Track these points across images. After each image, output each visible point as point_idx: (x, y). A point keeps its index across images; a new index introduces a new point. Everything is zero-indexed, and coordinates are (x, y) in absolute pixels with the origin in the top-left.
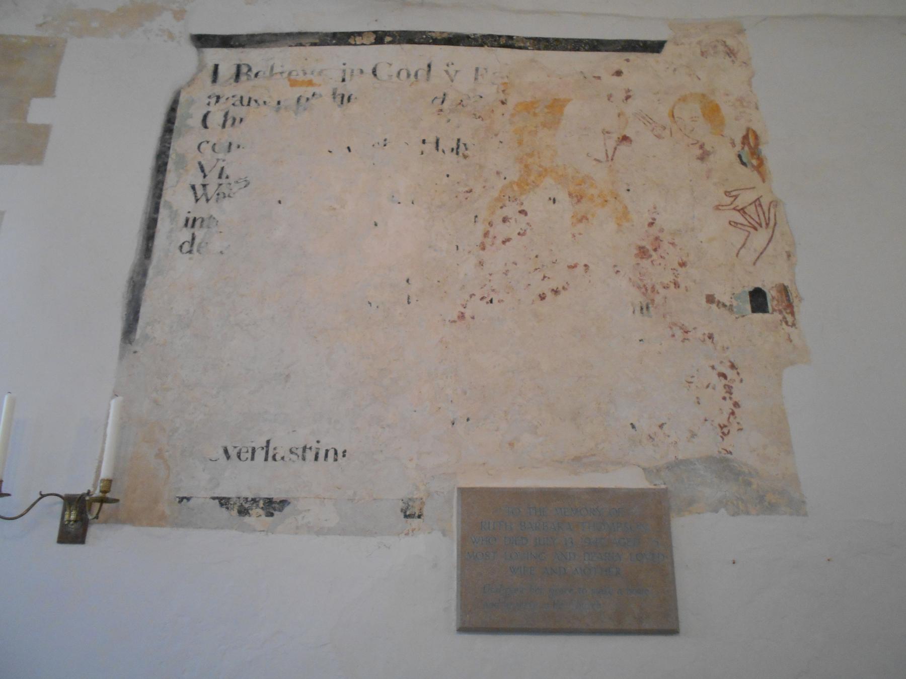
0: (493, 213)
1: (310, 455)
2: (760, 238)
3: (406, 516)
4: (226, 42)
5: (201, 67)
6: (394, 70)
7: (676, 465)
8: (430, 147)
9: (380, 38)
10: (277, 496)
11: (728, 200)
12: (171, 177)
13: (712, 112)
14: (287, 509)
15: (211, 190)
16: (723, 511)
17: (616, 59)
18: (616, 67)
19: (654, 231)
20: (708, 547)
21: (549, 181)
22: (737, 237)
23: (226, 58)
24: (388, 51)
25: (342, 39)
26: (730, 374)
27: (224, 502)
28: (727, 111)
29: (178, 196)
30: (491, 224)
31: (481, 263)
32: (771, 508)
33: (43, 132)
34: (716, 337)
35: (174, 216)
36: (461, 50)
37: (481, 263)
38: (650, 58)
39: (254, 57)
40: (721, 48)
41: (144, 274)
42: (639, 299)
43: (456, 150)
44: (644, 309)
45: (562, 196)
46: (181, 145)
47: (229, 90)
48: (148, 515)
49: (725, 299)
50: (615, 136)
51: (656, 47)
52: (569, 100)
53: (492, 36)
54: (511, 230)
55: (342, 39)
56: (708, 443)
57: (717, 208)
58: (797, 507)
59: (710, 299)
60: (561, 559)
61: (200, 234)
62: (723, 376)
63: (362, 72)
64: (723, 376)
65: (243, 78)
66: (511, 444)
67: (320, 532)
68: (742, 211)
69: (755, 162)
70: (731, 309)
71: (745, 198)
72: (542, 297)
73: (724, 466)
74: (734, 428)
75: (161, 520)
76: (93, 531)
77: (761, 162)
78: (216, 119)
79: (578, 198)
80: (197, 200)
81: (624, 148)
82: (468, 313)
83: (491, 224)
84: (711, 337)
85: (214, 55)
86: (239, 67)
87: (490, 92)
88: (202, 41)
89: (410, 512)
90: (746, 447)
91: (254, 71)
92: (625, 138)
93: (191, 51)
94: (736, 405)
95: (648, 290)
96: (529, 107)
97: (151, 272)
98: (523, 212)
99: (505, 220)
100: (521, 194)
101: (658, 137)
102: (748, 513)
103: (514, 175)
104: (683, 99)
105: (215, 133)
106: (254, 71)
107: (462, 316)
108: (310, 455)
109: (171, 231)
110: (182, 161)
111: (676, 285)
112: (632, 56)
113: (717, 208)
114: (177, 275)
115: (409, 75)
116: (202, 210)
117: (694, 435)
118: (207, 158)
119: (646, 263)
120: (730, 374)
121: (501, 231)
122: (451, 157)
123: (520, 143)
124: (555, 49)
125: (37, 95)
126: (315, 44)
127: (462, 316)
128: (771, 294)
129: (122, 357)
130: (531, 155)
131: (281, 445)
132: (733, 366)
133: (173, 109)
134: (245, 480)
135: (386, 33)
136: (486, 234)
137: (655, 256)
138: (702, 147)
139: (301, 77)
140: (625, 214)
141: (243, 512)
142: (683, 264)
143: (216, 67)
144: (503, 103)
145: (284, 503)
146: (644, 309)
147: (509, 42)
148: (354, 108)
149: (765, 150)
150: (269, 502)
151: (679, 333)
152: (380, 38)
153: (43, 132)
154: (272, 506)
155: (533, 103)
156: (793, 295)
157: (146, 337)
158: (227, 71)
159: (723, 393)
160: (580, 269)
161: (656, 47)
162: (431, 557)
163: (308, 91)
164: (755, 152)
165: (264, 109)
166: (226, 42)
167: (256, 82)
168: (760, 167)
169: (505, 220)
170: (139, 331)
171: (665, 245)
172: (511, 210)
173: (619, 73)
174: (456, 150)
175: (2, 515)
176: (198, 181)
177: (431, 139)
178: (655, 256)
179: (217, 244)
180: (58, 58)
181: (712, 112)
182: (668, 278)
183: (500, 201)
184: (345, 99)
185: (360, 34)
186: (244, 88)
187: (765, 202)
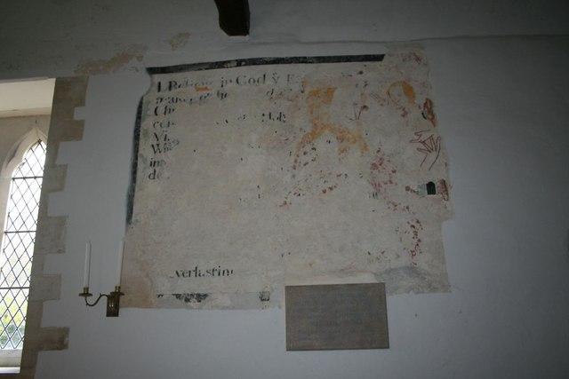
0: (299, 150)
1: (216, 273)
2: (432, 156)
3: (262, 300)
4: (164, 70)
5: (152, 85)
6: (247, 79)
7: (389, 271)
8: (267, 117)
9: (239, 63)
10: (201, 292)
11: (416, 137)
12: (142, 141)
13: (409, 91)
14: (207, 298)
15: (161, 147)
16: (411, 292)
17: (358, 66)
18: (360, 70)
19: (379, 155)
20: (401, 310)
21: (327, 132)
22: (421, 156)
23: (164, 79)
24: (243, 69)
25: (221, 65)
26: (417, 226)
27: (178, 296)
28: (416, 89)
29: (146, 151)
30: (298, 156)
31: (294, 176)
32: (434, 290)
33: (81, 123)
34: (411, 208)
35: (145, 161)
36: (281, 66)
37: (294, 176)
38: (377, 64)
39: (178, 77)
40: (413, 57)
41: (134, 190)
42: (372, 190)
43: (279, 119)
44: (375, 195)
45: (333, 139)
46: (147, 124)
47: (166, 94)
48: (144, 302)
49: (415, 188)
50: (360, 106)
51: (379, 58)
52: (336, 88)
53: (296, 58)
54: (308, 158)
55: (221, 65)
56: (405, 260)
57: (411, 141)
58: (446, 288)
59: (408, 189)
60: (340, 315)
61: (157, 169)
62: (413, 226)
63: (231, 81)
64: (413, 226)
65: (173, 88)
66: (311, 265)
67: (224, 308)
68: (424, 142)
69: (430, 117)
70: (417, 193)
71: (425, 136)
72: (324, 192)
73: (412, 270)
74: (418, 253)
75: (149, 306)
76: (122, 311)
77: (433, 116)
78: (161, 110)
79: (341, 139)
80: (155, 152)
81: (364, 112)
82: (288, 201)
83: (298, 156)
84: (407, 208)
85: (158, 78)
86: (170, 82)
87: (296, 88)
88: (152, 71)
89: (264, 298)
90: (423, 261)
91: (178, 84)
92: (365, 107)
93: (147, 77)
94: (419, 241)
95: (376, 186)
96: (315, 94)
97: (137, 189)
98: (314, 149)
99: (305, 154)
100: (313, 138)
101: (382, 105)
102: (423, 292)
103: (309, 130)
104: (394, 85)
105: (161, 118)
106: (178, 84)
107: (285, 203)
108: (216, 273)
109: (145, 168)
110: (146, 133)
111: (391, 182)
112: (368, 63)
113: (411, 141)
114: (150, 190)
115: (254, 81)
116: (159, 157)
117: (398, 256)
118: (158, 130)
119: (375, 172)
120: (417, 226)
121: (303, 159)
122: (277, 122)
123: (312, 113)
124: (328, 62)
125: (77, 105)
126: (206, 69)
127: (285, 203)
128: (437, 185)
129: (127, 230)
130: (317, 118)
131: (202, 269)
132: (418, 222)
133: (140, 107)
134: (186, 286)
135: (244, 60)
136: (296, 161)
137: (380, 168)
138: (403, 110)
139: (201, 86)
140: (365, 147)
141: (187, 300)
142: (394, 172)
143: (160, 83)
144: (302, 92)
145: (205, 296)
146: (375, 195)
147: (304, 60)
148: (228, 100)
149: (435, 110)
150: (199, 295)
151: (392, 206)
152: (239, 63)
153: (81, 123)
154: (200, 297)
155: (317, 91)
156: (448, 186)
157: (137, 221)
158: (165, 85)
159: (412, 235)
160: (343, 177)
161: (379, 58)
162: (275, 317)
163: (205, 93)
164: (430, 112)
165: (184, 103)
166: (164, 70)
167: (178, 90)
168: (433, 119)
169: (305, 154)
170: (133, 219)
171: (385, 162)
172: (308, 148)
173: (361, 73)
174: (279, 119)
175: (2, 364)
176: (155, 143)
177: (267, 114)
178: (380, 168)
179: (166, 174)
180: (86, 87)
181: (409, 91)
182: (386, 178)
183: (302, 145)
184: (223, 96)
185: (229, 62)
186: (174, 93)
187: (435, 137)
